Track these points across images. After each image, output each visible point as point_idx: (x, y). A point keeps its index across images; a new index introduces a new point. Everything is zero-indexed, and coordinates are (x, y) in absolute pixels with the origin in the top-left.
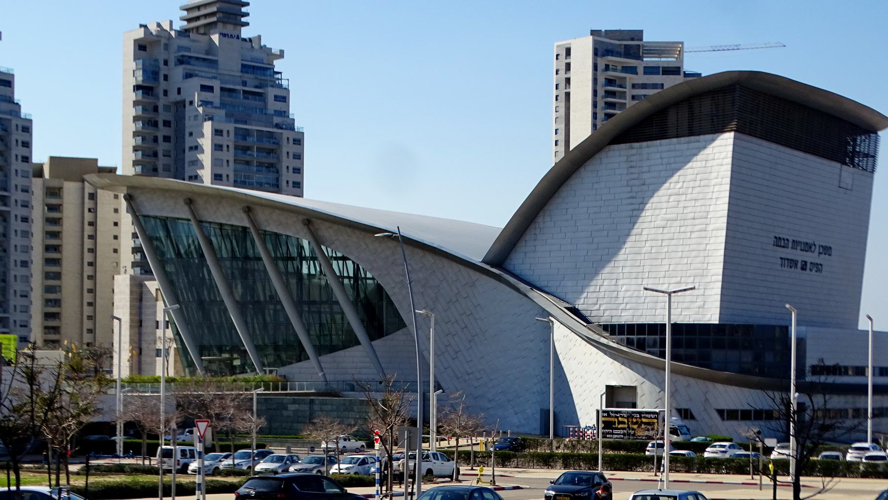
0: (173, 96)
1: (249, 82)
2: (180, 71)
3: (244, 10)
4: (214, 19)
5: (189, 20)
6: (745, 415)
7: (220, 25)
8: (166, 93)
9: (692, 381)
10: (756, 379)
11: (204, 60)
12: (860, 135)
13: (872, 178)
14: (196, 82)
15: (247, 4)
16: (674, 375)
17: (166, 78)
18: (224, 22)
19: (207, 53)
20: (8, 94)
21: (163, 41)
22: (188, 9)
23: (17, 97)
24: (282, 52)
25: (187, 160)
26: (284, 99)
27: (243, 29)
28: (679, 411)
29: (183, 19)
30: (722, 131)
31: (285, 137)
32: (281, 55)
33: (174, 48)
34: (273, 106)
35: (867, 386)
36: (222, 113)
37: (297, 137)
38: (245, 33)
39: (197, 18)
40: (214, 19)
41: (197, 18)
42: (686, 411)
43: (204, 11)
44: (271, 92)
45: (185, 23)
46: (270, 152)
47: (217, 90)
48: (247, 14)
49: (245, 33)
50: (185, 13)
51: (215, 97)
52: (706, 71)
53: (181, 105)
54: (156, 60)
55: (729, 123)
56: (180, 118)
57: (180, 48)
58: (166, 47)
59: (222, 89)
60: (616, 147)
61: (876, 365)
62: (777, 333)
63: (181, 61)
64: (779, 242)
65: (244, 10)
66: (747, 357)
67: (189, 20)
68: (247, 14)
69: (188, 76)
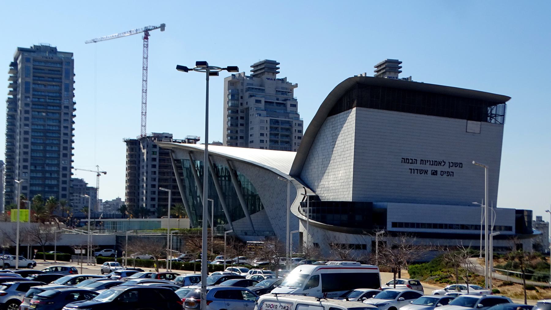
0: (245, 106)
1: (280, 99)
2: (247, 95)
3: (277, 66)
4: (263, 71)
5: (377, 72)
6: (351, 246)
7: (266, 73)
8: (242, 104)
9: (319, 229)
10: (345, 228)
11: (259, 89)
12: (490, 106)
13: (503, 127)
14: (253, 99)
15: (279, 64)
16: (496, 241)
17: (242, 97)
18: (390, 72)
19: (261, 86)
20: (295, 110)
21: (241, 81)
22: (377, 67)
23: (299, 111)
24: (297, 84)
25: (250, 134)
26: (295, 106)
27: (399, 74)
28: (314, 244)
29: (251, 71)
30: (352, 108)
31: (294, 122)
32: (296, 86)
33: (245, 84)
34: (289, 108)
35: (480, 235)
36: (265, 112)
37: (300, 123)
38: (278, 76)
39: (380, 70)
40: (263, 71)
41: (380, 70)
42: (317, 244)
43: (259, 68)
44: (289, 103)
45: (376, 73)
46: (288, 130)
47: (263, 102)
48: (401, 67)
49: (278, 76)
50: (253, 69)
51: (262, 105)
52: (417, 78)
53: (247, 109)
54: (238, 90)
55: (353, 104)
56: (247, 115)
57: (248, 84)
58: (242, 84)
59: (265, 102)
60: (331, 117)
61: (497, 225)
62: (526, 213)
63: (248, 89)
64: (405, 160)
65: (277, 66)
66: (345, 217)
67: (377, 72)
68: (401, 67)
69: (251, 96)
